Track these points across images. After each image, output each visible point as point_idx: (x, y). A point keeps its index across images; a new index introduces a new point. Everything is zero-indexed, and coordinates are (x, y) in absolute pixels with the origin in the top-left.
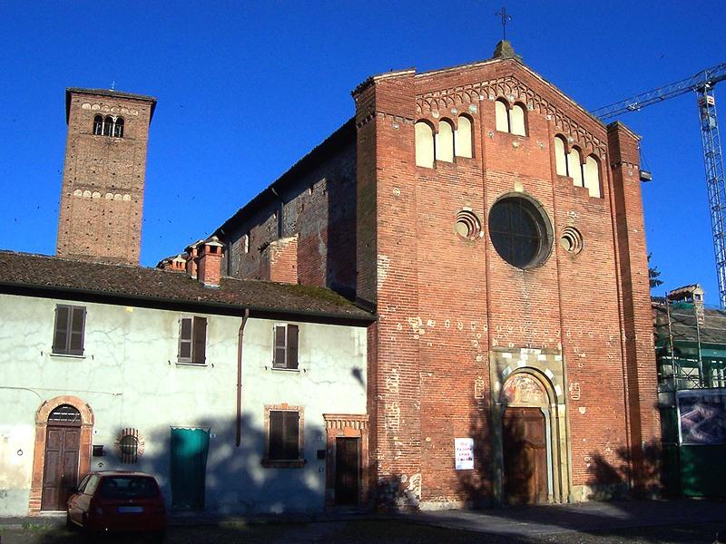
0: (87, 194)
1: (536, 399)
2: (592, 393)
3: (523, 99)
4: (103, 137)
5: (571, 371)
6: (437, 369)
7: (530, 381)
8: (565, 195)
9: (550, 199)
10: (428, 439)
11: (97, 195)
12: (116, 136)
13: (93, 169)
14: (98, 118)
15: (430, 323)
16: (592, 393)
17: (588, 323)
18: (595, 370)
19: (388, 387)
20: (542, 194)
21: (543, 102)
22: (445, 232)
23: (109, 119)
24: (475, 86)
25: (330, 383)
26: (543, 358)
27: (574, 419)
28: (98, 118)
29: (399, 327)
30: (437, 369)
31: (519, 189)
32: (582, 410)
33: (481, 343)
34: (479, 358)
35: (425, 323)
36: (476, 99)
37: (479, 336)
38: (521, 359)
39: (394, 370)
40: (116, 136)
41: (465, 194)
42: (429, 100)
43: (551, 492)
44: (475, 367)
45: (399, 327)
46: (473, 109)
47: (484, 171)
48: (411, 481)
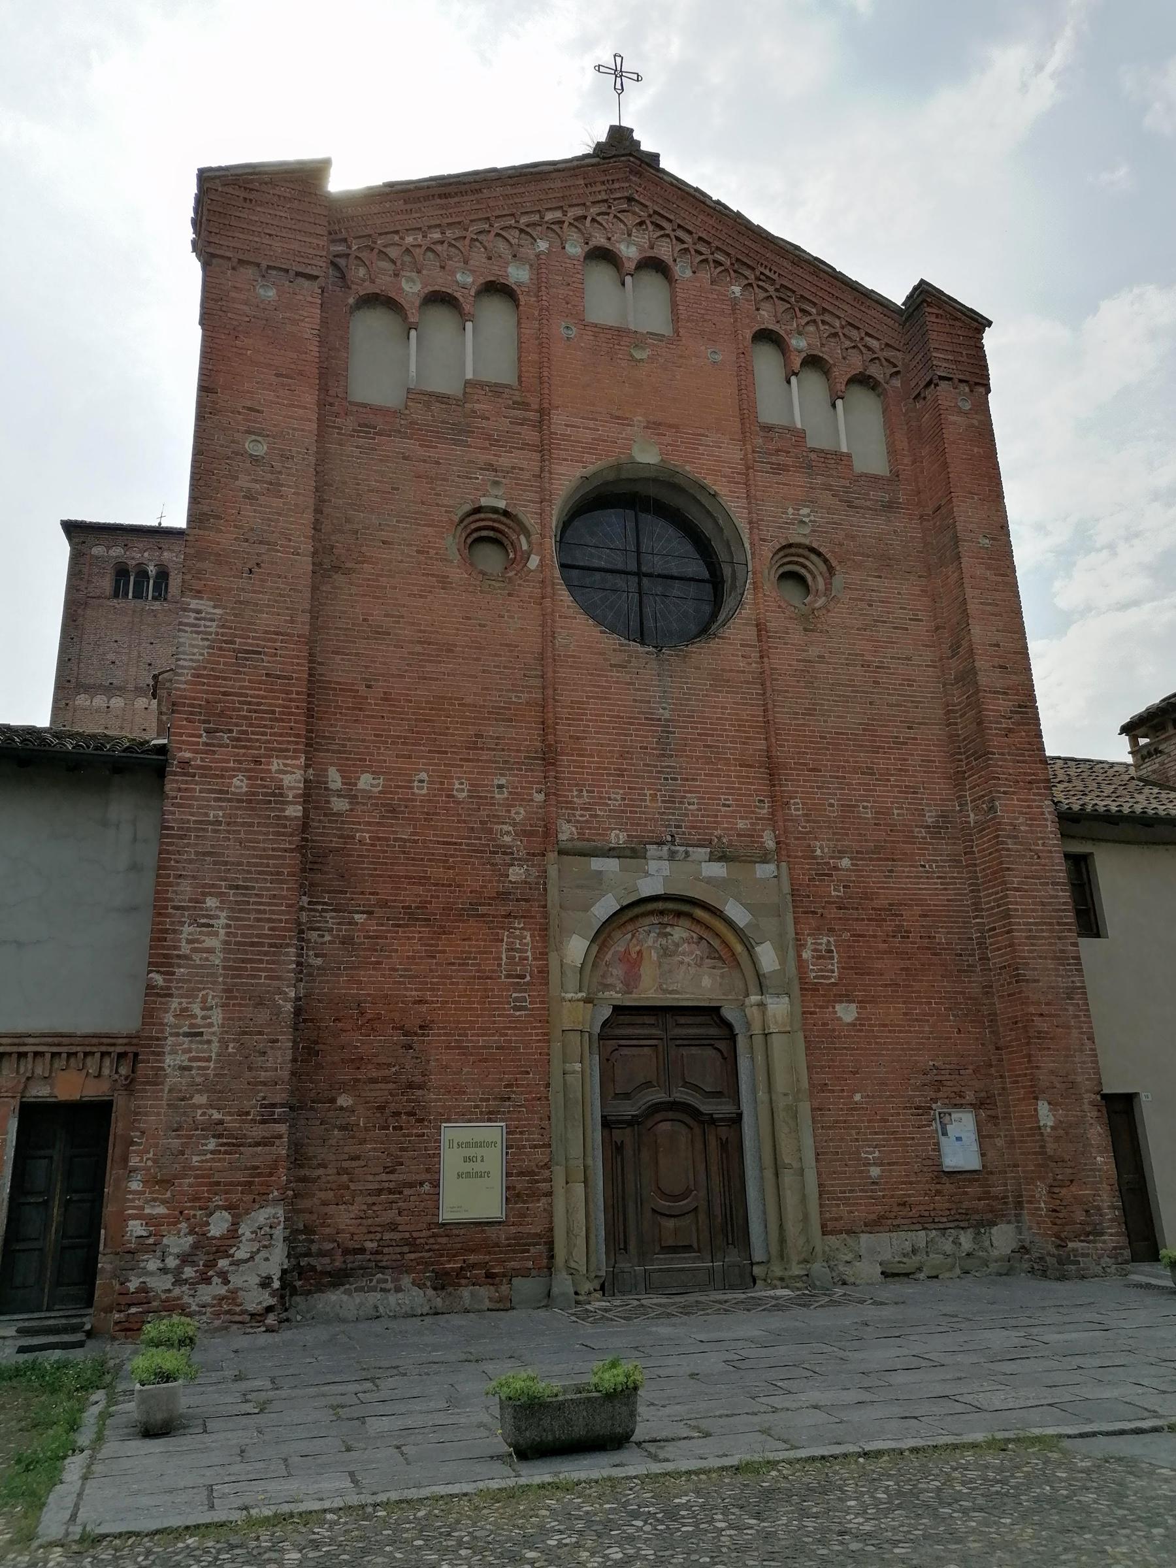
0: (100, 701)
1: (706, 982)
2: (878, 965)
3: (665, 251)
4: (131, 603)
5: (805, 905)
6: (384, 904)
7: (685, 935)
8: (779, 469)
9: (738, 478)
10: (344, 1101)
11: (117, 702)
12: (154, 598)
13: (111, 656)
14: (121, 572)
15: (365, 781)
16: (878, 965)
17: (856, 779)
18: (882, 902)
19: (185, 949)
20: (714, 465)
21: (719, 257)
22: (422, 557)
23: (143, 574)
24: (524, 220)
25: (19, 944)
26: (718, 870)
27: (819, 1039)
28: (121, 572)
29: (239, 784)
30: (384, 904)
31: (647, 455)
32: (847, 1013)
33: (525, 833)
34: (516, 873)
35: (350, 783)
36: (527, 252)
37: (520, 813)
38: (647, 874)
39: (211, 902)
40: (154, 598)
41: (490, 467)
42: (393, 252)
43: (64, 1321)
44: (503, 896)
45: (239, 784)
46: (518, 275)
47: (543, 412)
48: (245, 1230)
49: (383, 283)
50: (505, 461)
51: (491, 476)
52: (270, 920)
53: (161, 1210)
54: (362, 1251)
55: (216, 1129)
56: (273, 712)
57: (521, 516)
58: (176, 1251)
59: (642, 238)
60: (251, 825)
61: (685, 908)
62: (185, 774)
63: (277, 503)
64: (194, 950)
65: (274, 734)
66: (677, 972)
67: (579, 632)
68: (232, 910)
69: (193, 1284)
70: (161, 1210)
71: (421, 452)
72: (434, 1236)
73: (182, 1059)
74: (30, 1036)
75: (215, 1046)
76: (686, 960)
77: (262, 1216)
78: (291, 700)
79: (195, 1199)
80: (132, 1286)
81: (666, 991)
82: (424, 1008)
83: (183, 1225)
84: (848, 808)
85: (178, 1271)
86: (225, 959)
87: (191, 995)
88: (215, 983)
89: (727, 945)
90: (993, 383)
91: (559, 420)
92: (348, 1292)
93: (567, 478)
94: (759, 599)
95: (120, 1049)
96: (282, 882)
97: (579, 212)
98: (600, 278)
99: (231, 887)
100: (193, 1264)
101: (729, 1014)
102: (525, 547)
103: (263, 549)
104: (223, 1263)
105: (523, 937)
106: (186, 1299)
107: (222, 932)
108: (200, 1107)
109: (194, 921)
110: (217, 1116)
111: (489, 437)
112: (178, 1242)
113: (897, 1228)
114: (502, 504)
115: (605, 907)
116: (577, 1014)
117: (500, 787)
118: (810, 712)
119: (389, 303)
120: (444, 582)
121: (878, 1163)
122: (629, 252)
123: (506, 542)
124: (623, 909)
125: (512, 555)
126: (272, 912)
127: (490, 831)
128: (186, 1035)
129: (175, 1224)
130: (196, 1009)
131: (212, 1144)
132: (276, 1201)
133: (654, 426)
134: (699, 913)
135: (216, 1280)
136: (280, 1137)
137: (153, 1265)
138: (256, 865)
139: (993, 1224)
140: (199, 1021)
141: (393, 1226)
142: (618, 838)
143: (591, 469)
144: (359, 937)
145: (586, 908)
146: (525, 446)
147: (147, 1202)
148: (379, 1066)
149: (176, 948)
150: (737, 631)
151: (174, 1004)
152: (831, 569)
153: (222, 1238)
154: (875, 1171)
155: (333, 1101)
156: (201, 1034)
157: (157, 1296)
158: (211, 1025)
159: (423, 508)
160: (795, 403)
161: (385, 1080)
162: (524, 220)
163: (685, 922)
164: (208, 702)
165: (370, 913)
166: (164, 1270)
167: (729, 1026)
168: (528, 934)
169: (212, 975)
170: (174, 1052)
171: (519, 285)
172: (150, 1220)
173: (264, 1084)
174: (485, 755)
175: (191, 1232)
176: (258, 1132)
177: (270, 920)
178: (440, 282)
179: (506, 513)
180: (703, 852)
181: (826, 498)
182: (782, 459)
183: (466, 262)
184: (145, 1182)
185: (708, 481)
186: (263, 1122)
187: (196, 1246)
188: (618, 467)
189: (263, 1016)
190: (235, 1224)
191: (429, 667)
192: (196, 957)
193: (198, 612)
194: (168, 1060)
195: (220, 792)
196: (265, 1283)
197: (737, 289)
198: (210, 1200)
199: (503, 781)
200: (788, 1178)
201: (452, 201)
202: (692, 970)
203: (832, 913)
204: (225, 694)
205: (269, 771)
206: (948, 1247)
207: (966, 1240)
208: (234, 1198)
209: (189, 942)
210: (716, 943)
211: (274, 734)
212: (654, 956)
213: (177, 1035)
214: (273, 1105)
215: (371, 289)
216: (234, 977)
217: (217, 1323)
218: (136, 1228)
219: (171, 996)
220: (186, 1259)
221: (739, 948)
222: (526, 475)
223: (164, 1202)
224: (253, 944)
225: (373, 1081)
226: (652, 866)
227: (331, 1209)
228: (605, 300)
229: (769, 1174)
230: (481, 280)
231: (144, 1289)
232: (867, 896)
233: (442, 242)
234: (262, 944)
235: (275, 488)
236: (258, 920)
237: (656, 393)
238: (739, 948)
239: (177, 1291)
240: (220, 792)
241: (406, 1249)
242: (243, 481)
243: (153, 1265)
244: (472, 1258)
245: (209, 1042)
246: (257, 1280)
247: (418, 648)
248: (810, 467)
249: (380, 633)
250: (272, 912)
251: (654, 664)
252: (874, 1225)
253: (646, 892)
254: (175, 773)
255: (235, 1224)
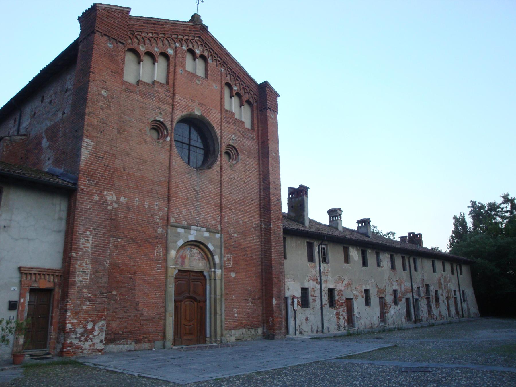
3: (206, 54)
5: (227, 246)
10: (114, 292)
15: (122, 199)
17: (239, 213)
19: (81, 246)
20: (213, 118)
22: (140, 132)
24: (173, 36)
26: (207, 234)
27: (228, 281)
29: (96, 198)
30: (126, 236)
31: (197, 113)
32: (233, 275)
34: (159, 230)
35: (118, 199)
36: (173, 45)
37: (161, 213)
38: (191, 234)
39: (88, 233)
41: (159, 108)
42: (139, 37)
44: (156, 237)
46: (170, 52)
48: (96, 328)
49: (135, 46)
50: (164, 107)
51: (159, 111)
52: (103, 240)
53: (76, 321)
54: (119, 334)
55: (89, 299)
56: (105, 177)
57: (166, 124)
58: (79, 332)
59: (200, 48)
60: (99, 211)
61: (198, 244)
62: (82, 193)
63: (109, 111)
64: (84, 247)
65: (106, 184)
66: (195, 262)
67: (178, 162)
68: (93, 236)
69: (84, 342)
70: (76, 321)
71: (142, 100)
72: (136, 330)
73: (81, 279)
74: (34, 268)
75: (89, 275)
76: (196, 258)
77: (101, 323)
78: (110, 174)
79: (84, 318)
80: (68, 341)
81: (191, 266)
82: (135, 268)
83: (81, 326)
84: (237, 221)
85: (79, 338)
86: (92, 250)
87: (83, 260)
88: (89, 257)
89: (207, 254)
90: (279, 112)
91: (177, 97)
92: (114, 344)
93: (178, 115)
94: (222, 160)
95: (57, 274)
96: (106, 228)
97: (187, 37)
98: (189, 57)
99: (93, 229)
100: (84, 336)
101: (206, 274)
102: (166, 133)
103: (105, 125)
104: (91, 336)
105: (160, 249)
106: (82, 345)
107: (91, 242)
108: (85, 292)
109: (84, 237)
110: (89, 295)
111: (159, 99)
112: (80, 330)
113: (239, 329)
114: (161, 120)
115: (180, 243)
116: (173, 272)
117: (157, 205)
118: (231, 193)
119: (135, 52)
120: (145, 141)
121: (237, 313)
122: (198, 52)
123: (159, 131)
124: (185, 243)
125: (160, 135)
126: (104, 237)
127: (153, 218)
128: (82, 272)
129: (79, 325)
130: (84, 265)
131: (88, 303)
132: (104, 320)
133: (200, 104)
134: (201, 246)
135: (89, 340)
136: (105, 302)
137: (73, 336)
138: (100, 223)
139: (258, 327)
140: (85, 268)
141: (126, 328)
142: (184, 223)
143: (184, 114)
144: (119, 246)
145: (176, 242)
146: (168, 104)
147: (72, 319)
148: (123, 283)
149: (79, 246)
150: (216, 167)
151: (79, 262)
152: (238, 153)
153: (91, 329)
154: (236, 315)
155: (111, 292)
156: (85, 272)
157: (75, 345)
158: (88, 269)
159: (141, 117)
160: (232, 105)
161: (125, 287)
162: (173, 36)
163: (196, 248)
164: (89, 171)
165: (122, 239)
166: (76, 338)
167: (205, 276)
168: (161, 248)
169: (89, 255)
170: (78, 276)
171: (171, 55)
172: (72, 324)
173: (101, 287)
174: (153, 195)
175: (83, 327)
176: (100, 300)
177: (103, 240)
178: (150, 49)
179: (162, 123)
180: (204, 229)
181: (238, 133)
182: (229, 120)
183: (157, 45)
184: (71, 313)
185: (212, 123)
186: (101, 298)
187: (85, 331)
188: (190, 114)
189: (101, 268)
190: (94, 325)
191: (140, 167)
192: (84, 249)
193: (87, 143)
194: (77, 279)
195: (91, 200)
196: (101, 341)
197: (223, 69)
198: (88, 319)
199: (157, 203)
200: (218, 317)
201: (156, 26)
202: (197, 261)
203: (232, 248)
204: (93, 169)
205: (104, 195)
206: (249, 333)
207: (253, 331)
208: (94, 318)
209: (83, 244)
210: (204, 254)
211: (106, 184)
212: (189, 256)
213: (79, 271)
214: (103, 293)
215: (131, 46)
216: (94, 256)
217: (90, 352)
218: (69, 326)
219: (77, 260)
220: (82, 335)
221: (210, 256)
222: (168, 112)
223: (76, 319)
224: (99, 246)
225: (121, 287)
226: (192, 232)
227: (111, 322)
228: (189, 64)
229: (213, 316)
230: (161, 51)
231: (71, 343)
232: (240, 245)
233: (152, 37)
234: (101, 247)
235: (109, 107)
236: (100, 239)
237: (200, 94)
238: (210, 256)
239: (80, 343)
240: (91, 200)
241: (129, 333)
242: (101, 104)
243: (73, 336)
244: (145, 336)
245: (87, 274)
246: (99, 341)
247: (138, 160)
248: (235, 124)
249: (128, 154)
250: (104, 237)
251: (196, 174)
252: (235, 328)
253: (190, 239)
254: (79, 193)
255: (94, 325)
